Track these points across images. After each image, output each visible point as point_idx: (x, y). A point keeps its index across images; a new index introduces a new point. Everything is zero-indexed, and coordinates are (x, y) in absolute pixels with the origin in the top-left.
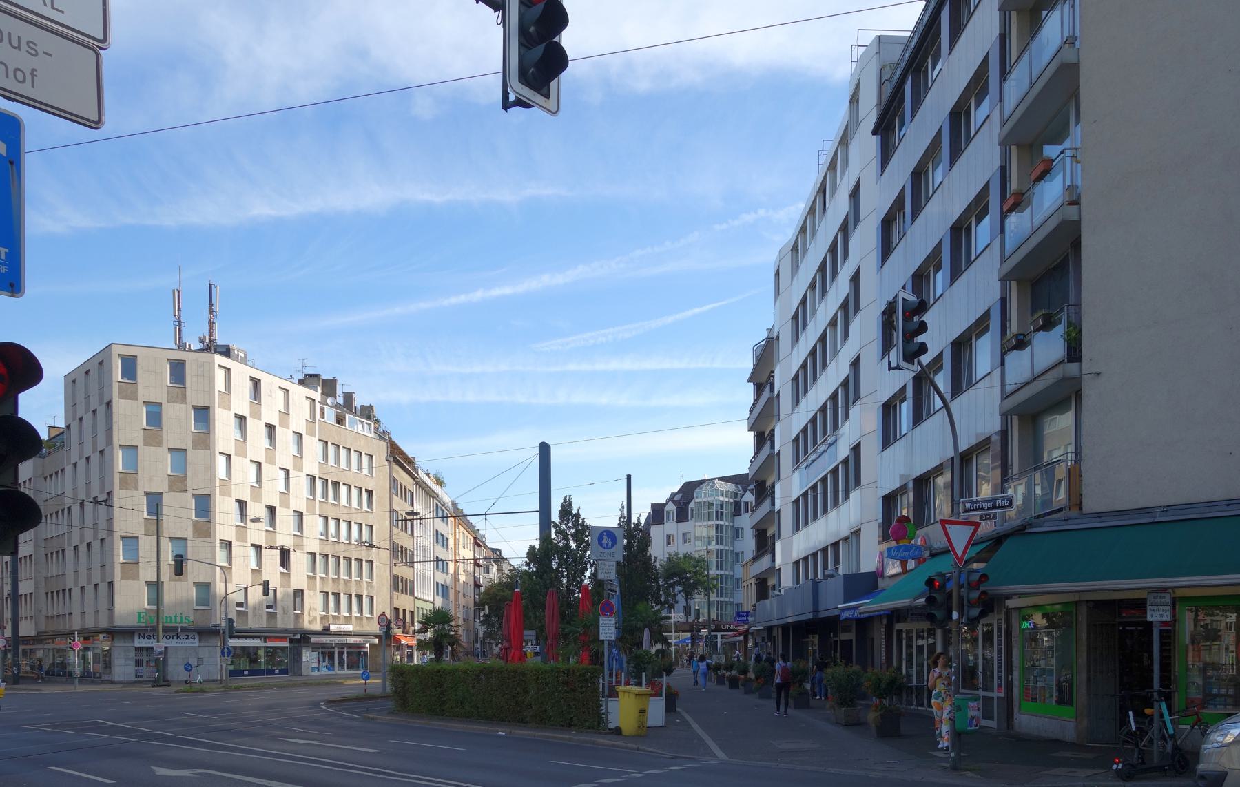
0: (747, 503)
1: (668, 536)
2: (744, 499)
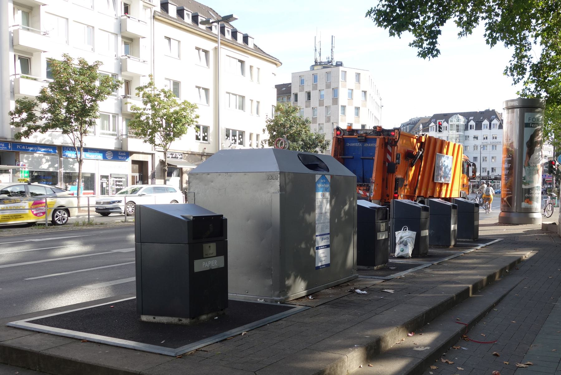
0: (471, 126)
1: (475, 138)
2: (470, 124)
